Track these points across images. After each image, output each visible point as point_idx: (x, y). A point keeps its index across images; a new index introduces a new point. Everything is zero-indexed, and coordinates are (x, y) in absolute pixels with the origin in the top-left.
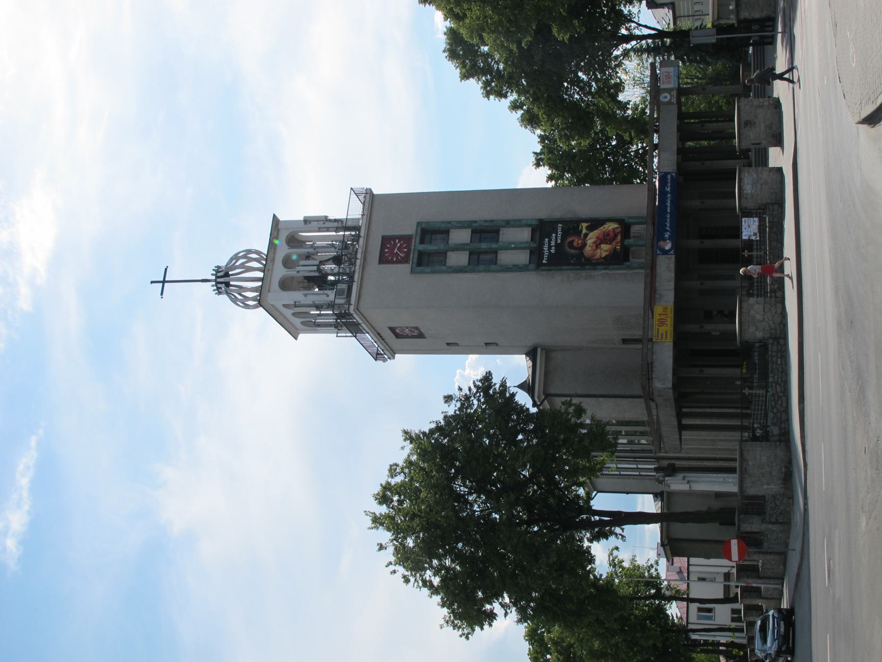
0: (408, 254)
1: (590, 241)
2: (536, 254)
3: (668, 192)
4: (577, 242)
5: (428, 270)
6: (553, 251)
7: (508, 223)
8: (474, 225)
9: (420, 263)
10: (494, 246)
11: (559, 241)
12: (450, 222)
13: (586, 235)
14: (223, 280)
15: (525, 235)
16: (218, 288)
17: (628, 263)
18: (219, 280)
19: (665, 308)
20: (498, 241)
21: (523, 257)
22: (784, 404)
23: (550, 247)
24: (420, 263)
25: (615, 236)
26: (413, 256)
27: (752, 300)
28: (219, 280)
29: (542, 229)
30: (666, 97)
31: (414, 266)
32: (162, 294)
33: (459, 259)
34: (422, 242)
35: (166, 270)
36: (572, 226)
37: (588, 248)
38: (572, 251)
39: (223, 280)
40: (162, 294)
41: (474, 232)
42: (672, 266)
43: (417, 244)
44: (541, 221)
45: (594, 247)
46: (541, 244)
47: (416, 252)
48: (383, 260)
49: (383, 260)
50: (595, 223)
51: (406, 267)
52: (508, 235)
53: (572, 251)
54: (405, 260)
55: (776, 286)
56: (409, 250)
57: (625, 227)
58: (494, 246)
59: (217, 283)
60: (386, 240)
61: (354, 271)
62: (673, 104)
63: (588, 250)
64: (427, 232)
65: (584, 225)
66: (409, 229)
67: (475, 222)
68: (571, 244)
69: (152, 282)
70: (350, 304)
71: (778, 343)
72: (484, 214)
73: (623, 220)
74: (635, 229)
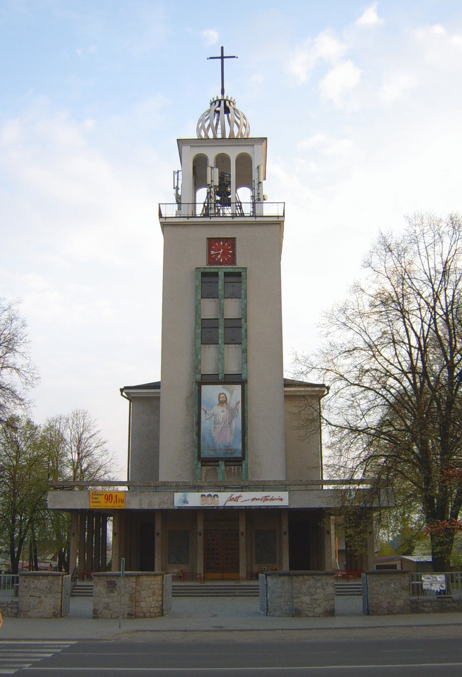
5: (198, 283)
9: (204, 275)
10: (220, 341)
14: (223, 107)
16: (215, 102)
17: (200, 465)
18: (222, 102)
19: (122, 501)
24: (204, 275)
26: (213, 268)
28: (222, 102)
31: (203, 270)
32: (211, 58)
33: (209, 308)
34: (226, 275)
35: (234, 57)
39: (223, 107)
40: (211, 58)
43: (224, 270)
47: (216, 270)
49: (212, 242)
52: (232, 352)
54: (211, 260)
56: (220, 264)
59: (220, 102)
60: (232, 241)
61: (211, 217)
64: (237, 277)
66: (241, 262)
67: (246, 321)
69: (222, 48)
72: (254, 328)
73: (244, 459)
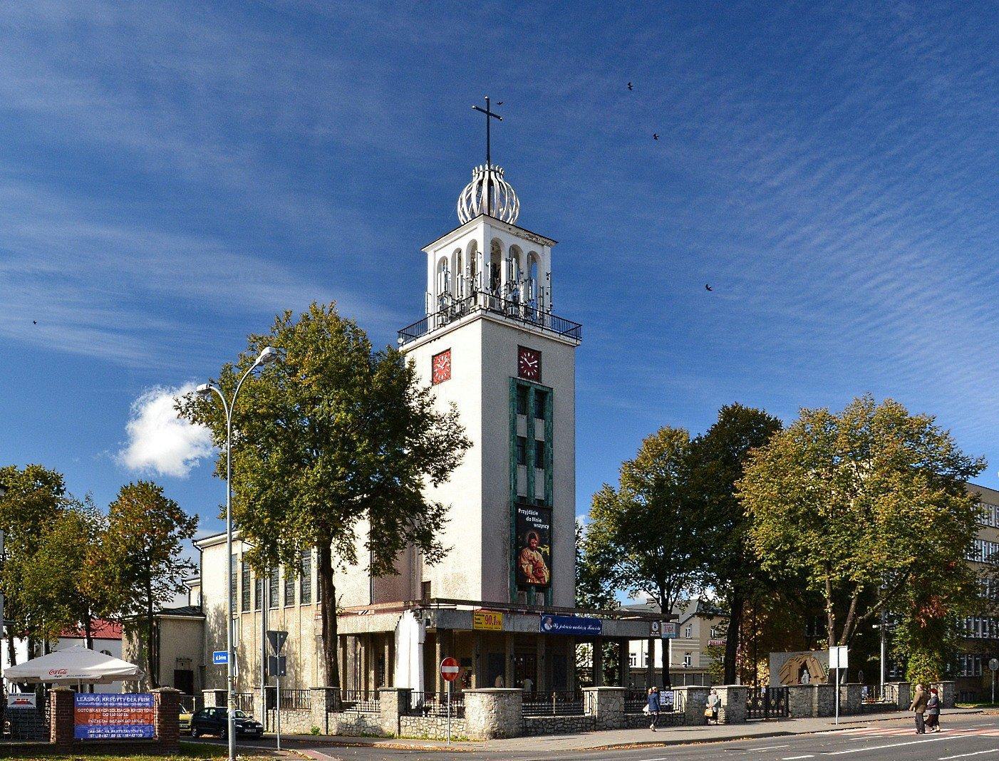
0: (526, 376)
1: (535, 554)
2: (522, 502)
3: (587, 627)
4: (535, 542)
6: (527, 519)
7: (549, 480)
8: (549, 445)
11: (535, 525)
12: (552, 421)
13: (540, 551)
15: (540, 494)
20: (536, 467)
21: (522, 491)
22: (549, 731)
23: (531, 516)
25: (539, 578)
27: (622, 700)
29: (545, 509)
30: (655, 627)
31: (518, 381)
34: (537, 391)
36: (547, 538)
37: (529, 552)
38: (527, 538)
41: (523, 439)
42: (532, 630)
44: (551, 509)
45: (530, 558)
46: (533, 508)
48: (522, 350)
49: (522, 350)
50: (549, 560)
51: (515, 373)
53: (527, 538)
54: (521, 373)
55: (631, 721)
57: (545, 588)
58: (532, 462)
60: (537, 355)
62: (650, 633)
63: (528, 552)
65: (548, 550)
68: (532, 536)
70: (506, 317)
71: (592, 724)
74: (541, 596)
